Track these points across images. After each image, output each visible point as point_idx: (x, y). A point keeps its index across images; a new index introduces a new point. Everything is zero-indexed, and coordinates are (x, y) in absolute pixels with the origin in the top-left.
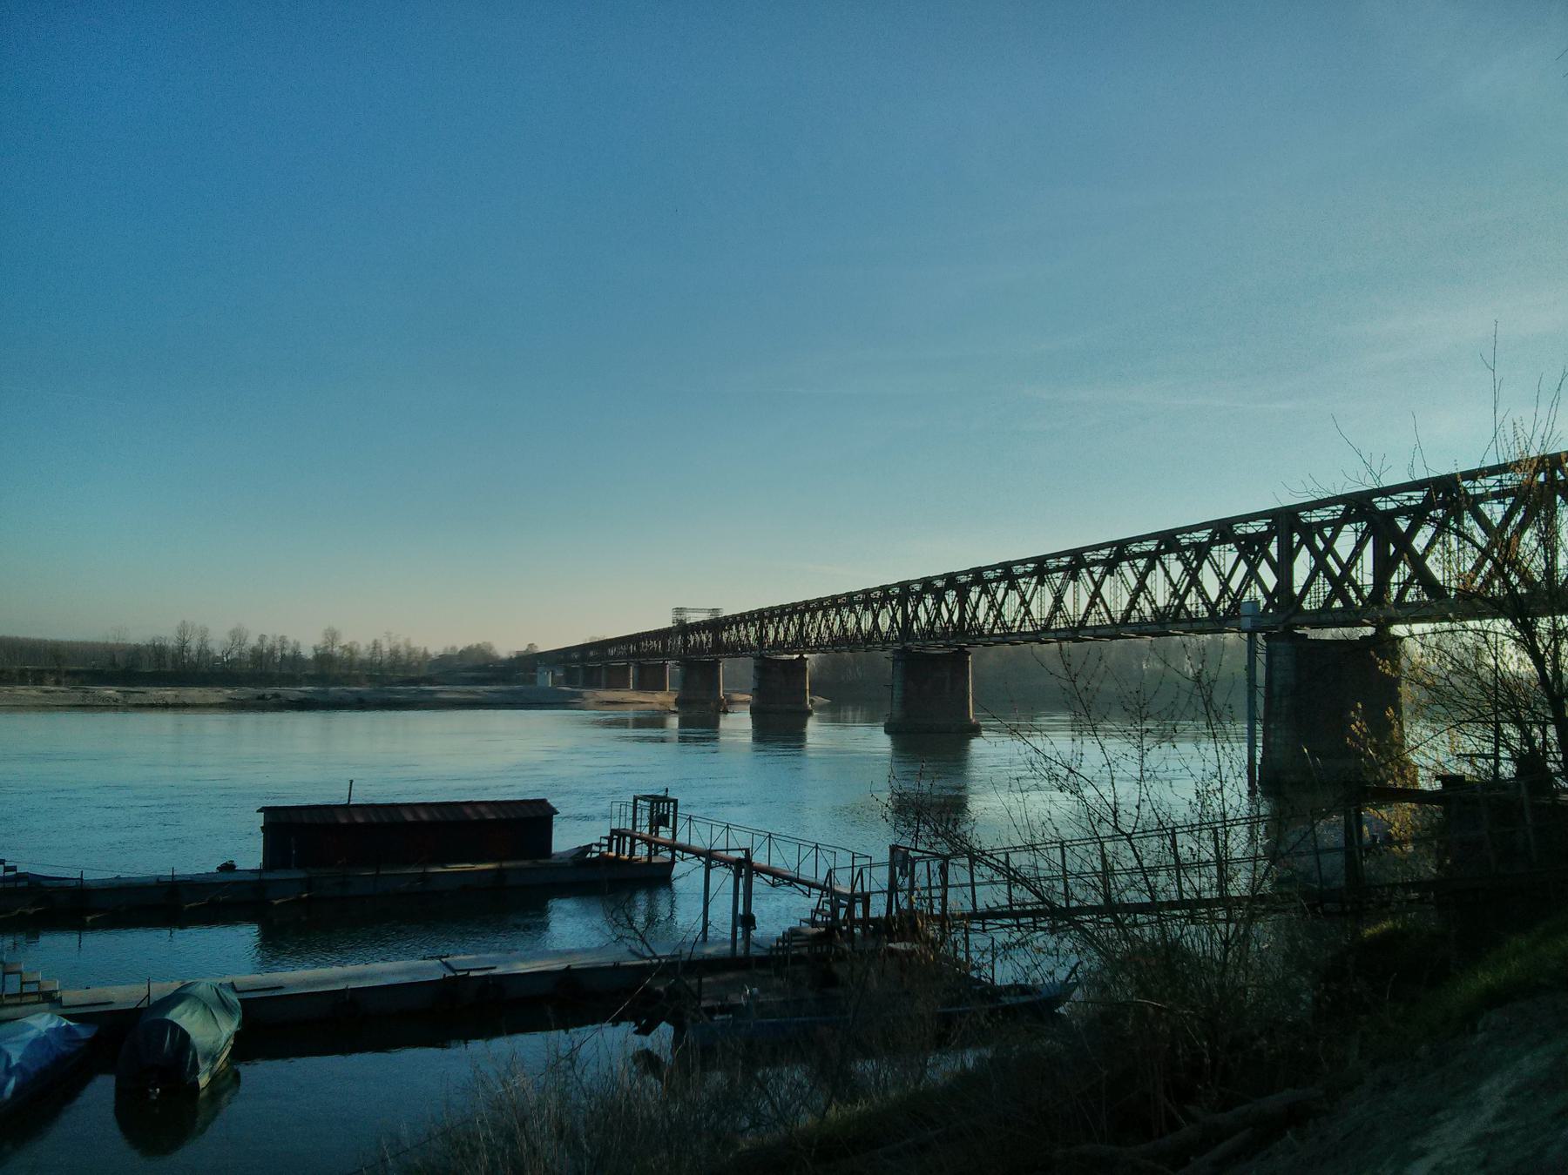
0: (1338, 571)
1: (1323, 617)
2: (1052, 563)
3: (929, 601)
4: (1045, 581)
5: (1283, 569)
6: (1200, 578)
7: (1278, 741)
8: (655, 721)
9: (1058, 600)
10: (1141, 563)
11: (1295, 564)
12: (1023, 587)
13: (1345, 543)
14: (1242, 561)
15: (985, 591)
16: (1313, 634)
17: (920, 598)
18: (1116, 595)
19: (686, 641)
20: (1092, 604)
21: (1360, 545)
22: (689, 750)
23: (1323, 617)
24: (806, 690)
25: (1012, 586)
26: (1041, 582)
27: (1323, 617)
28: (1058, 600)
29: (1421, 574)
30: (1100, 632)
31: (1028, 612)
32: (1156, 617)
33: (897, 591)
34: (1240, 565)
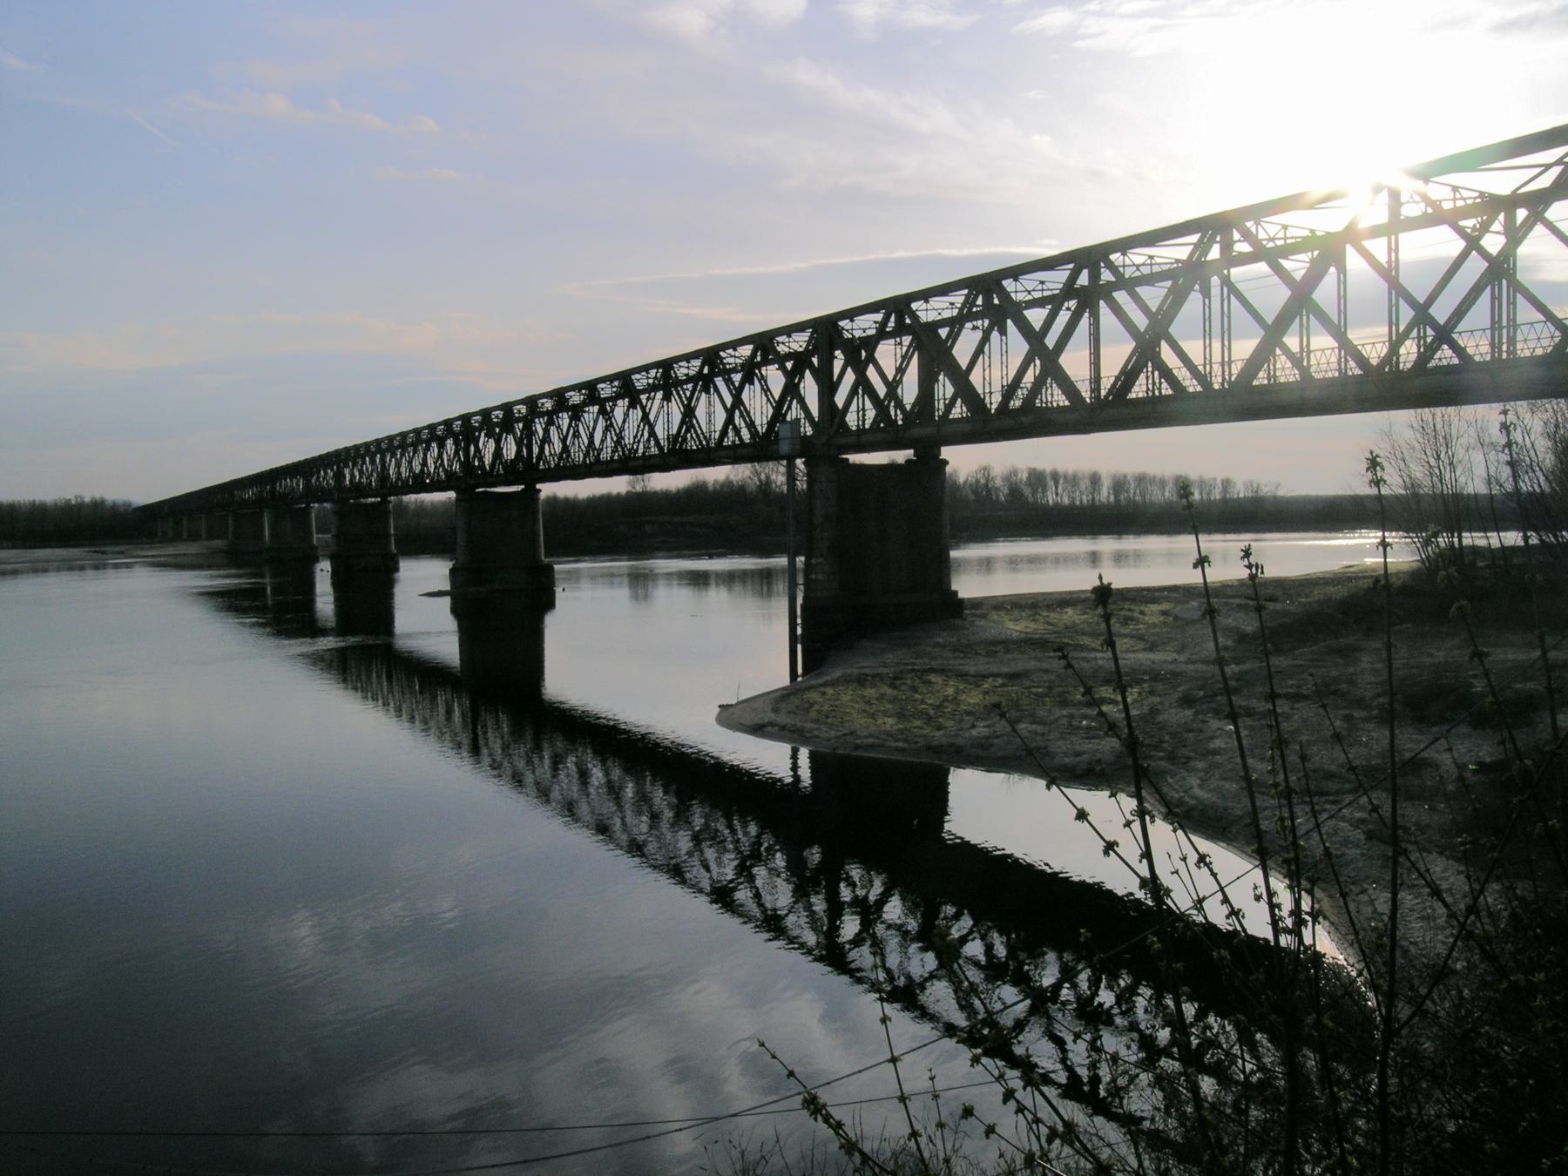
0: (881, 390)
1: (1026, 420)
2: (681, 371)
3: (564, 420)
4: (672, 394)
5: (828, 387)
6: (802, 392)
7: (820, 577)
8: (1266, 485)
9: (689, 412)
10: (737, 378)
11: (816, 387)
12: (644, 402)
13: (887, 355)
14: (849, 369)
15: (633, 404)
16: (856, 458)
17: (551, 417)
18: (711, 414)
19: (339, 476)
20: (730, 420)
21: (906, 358)
22: (1371, 535)
23: (1026, 420)
24: (389, 535)
25: (633, 404)
26: (667, 398)
27: (865, 441)
28: (689, 412)
29: (965, 390)
30: (740, 452)
31: (652, 434)
32: (755, 440)
33: (523, 409)
34: (968, 360)
